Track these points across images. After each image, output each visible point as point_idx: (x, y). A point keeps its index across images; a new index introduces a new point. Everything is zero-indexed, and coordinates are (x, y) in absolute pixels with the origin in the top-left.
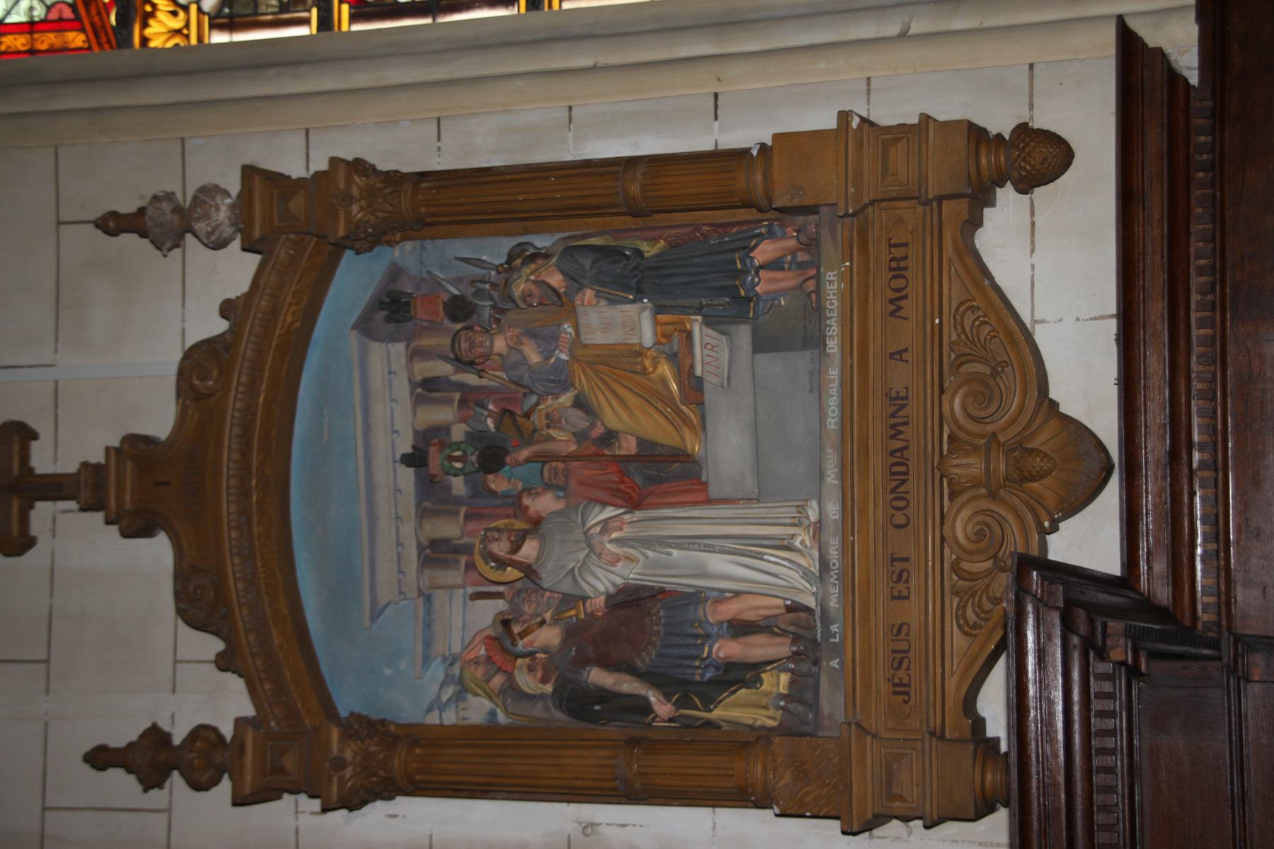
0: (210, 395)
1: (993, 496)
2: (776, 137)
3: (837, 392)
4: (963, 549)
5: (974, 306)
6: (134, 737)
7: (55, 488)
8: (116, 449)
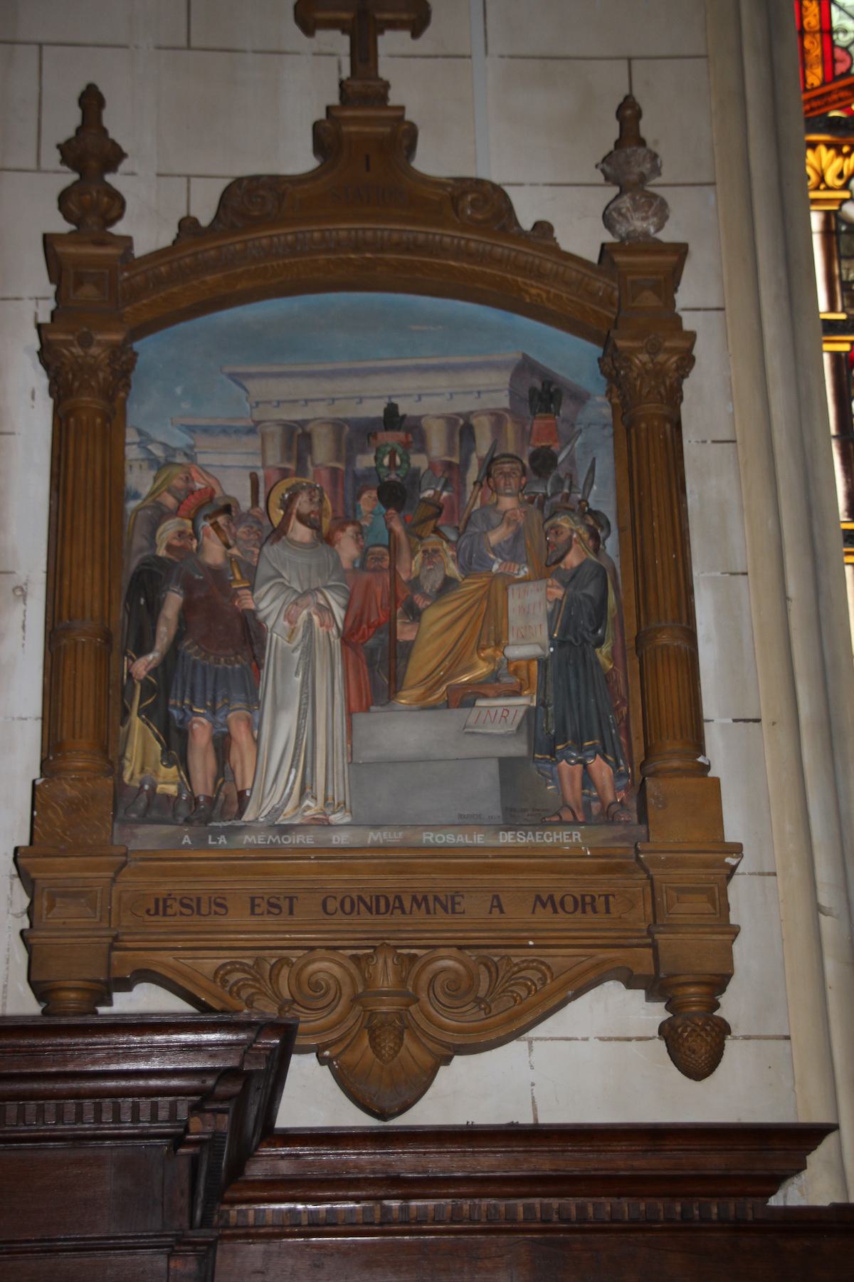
1: (355, 999)
2: (716, 781)
3: (460, 842)
4: (301, 970)
6: (112, 135)
7: (363, 55)
8: (402, 117)
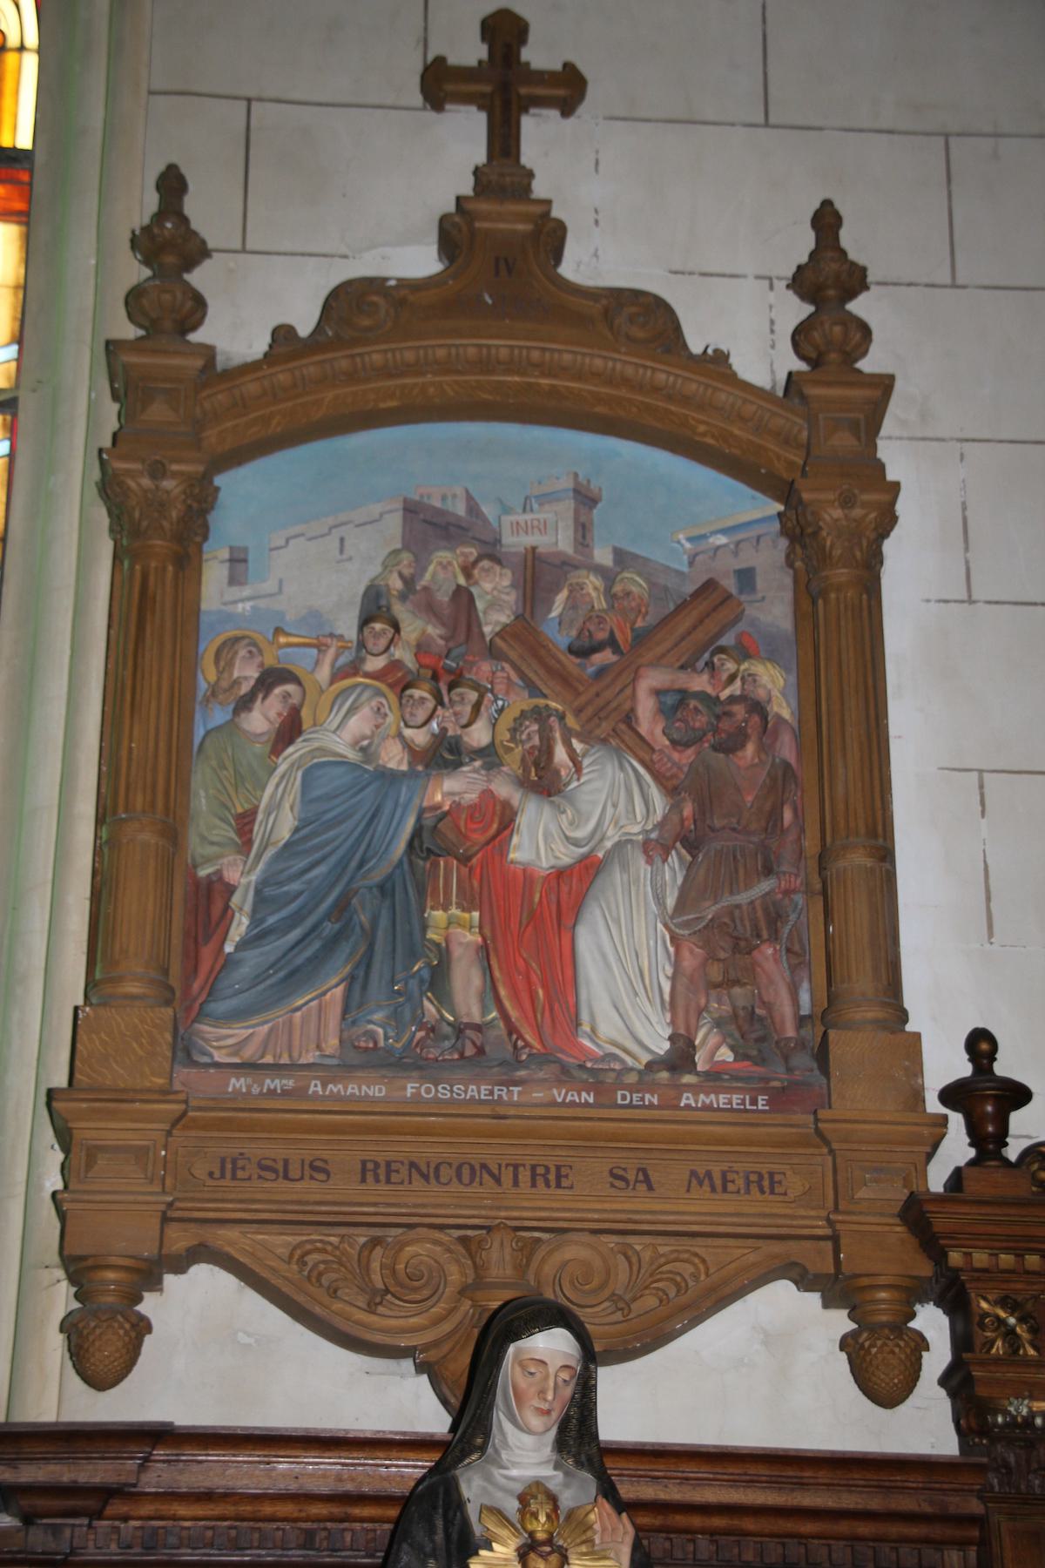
0: (611, 328)
5: (700, 1275)
7: (503, 141)
8: (548, 213)
